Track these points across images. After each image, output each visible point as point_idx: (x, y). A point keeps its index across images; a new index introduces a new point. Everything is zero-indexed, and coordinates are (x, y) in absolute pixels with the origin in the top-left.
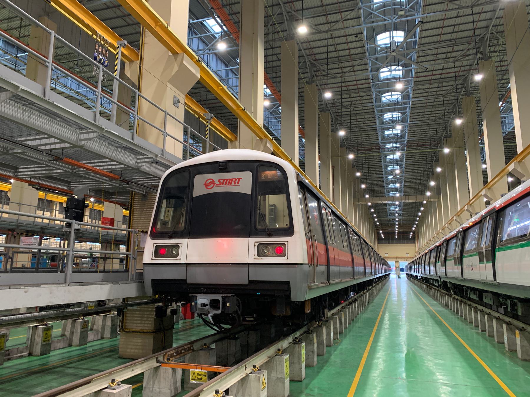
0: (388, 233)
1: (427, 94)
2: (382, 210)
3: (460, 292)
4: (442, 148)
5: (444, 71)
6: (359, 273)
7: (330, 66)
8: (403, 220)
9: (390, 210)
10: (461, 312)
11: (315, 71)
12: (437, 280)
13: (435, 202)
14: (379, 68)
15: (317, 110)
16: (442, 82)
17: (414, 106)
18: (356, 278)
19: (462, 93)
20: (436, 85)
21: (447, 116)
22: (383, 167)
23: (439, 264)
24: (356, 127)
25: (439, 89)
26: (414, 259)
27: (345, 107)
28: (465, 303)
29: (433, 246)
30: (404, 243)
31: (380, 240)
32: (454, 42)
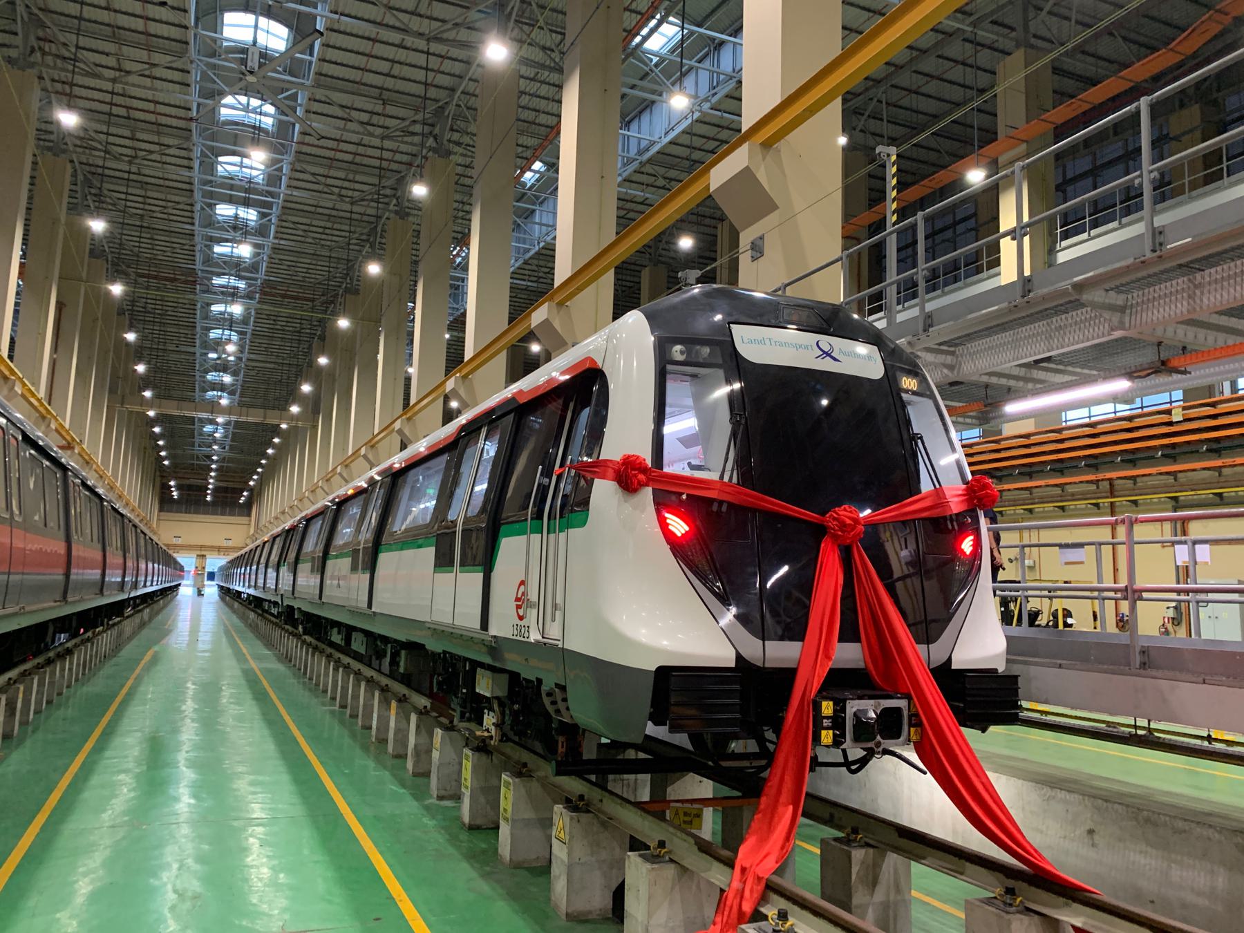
0: (190, 487)
1: (316, 187)
2: (181, 432)
3: (305, 630)
4: (336, 314)
5: (361, 150)
6: (85, 585)
7: (83, 42)
8: (230, 460)
9: (201, 434)
10: (312, 671)
11: (39, 39)
12: (275, 603)
13: (305, 430)
14: (222, 94)
15: (30, 148)
16: (356, 172)
17: (289, 205)
18: (70, 600)
19: (391, 207)
20: (342, 174)
21: (357, 248)
22: (198, 329)
23: (284, 570)
24: (142, 216)
25: (346, 184)
26: (243, 552)
27: (117, 158)
28: (322, 652)
29: (280, 529)
30: (223, 514)
31: (166, 503)
32: (383, 96)
